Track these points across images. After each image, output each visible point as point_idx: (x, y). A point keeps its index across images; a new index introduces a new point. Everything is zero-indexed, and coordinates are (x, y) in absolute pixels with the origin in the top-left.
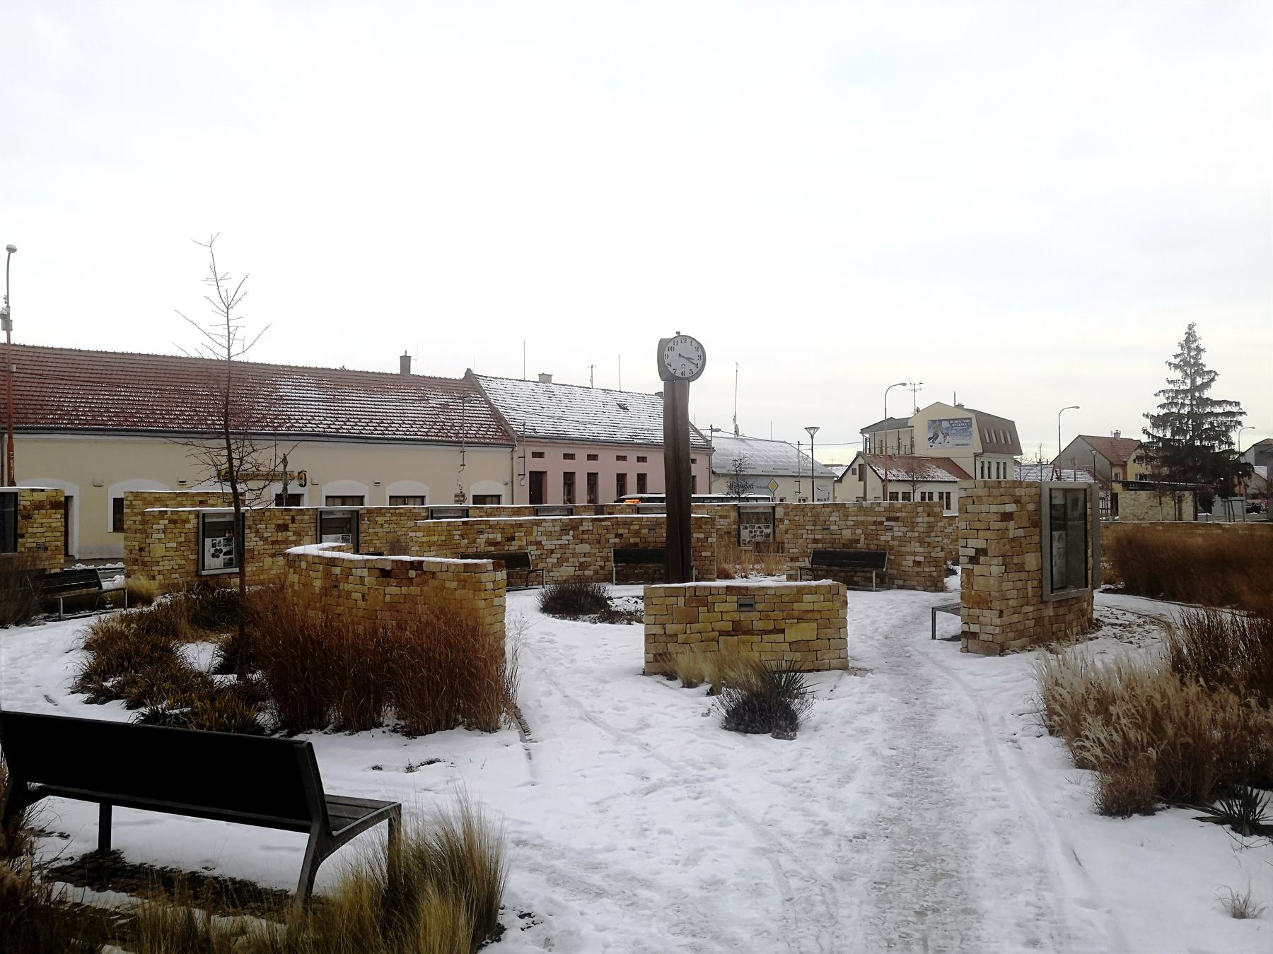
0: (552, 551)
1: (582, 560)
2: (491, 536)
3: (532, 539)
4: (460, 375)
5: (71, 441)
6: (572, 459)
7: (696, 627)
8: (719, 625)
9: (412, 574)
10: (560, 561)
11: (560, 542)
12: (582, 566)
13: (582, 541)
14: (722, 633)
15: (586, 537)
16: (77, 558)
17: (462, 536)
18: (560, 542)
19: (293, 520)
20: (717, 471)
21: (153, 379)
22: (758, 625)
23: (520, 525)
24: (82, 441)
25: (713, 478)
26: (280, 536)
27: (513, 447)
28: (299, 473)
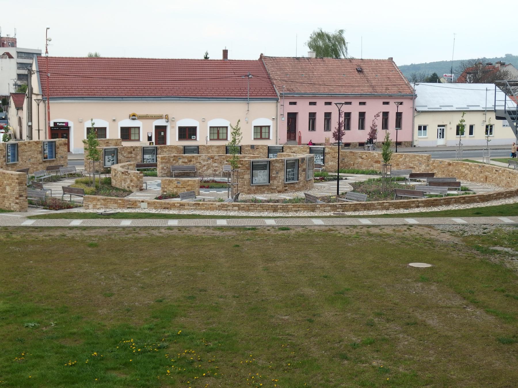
0: (205, 165)
1: (215, 168)
2: (183, 160)
3: (198, 161)
4: (257, 58)
5: (72, 103)
6: (315, 105)
7: (170, 186)
8: (174, 186)
9: (126, 173)
10: (208, 169)
11: (208, 162)
12: (215, 170)
13: (215, 162)
14: (174, 188)
15: (216, 161)
16: (73, 153)
17: (174, 160)
18: (208, 162)
19: (134, 150)
20: (419, 109)
21: (103, 68)
22: (181, 186)
23: (194, 157)
24: (74, 103)
25: (416, 114)
26: (130, 155)
27: (277, 100)
28: (166, 115)
